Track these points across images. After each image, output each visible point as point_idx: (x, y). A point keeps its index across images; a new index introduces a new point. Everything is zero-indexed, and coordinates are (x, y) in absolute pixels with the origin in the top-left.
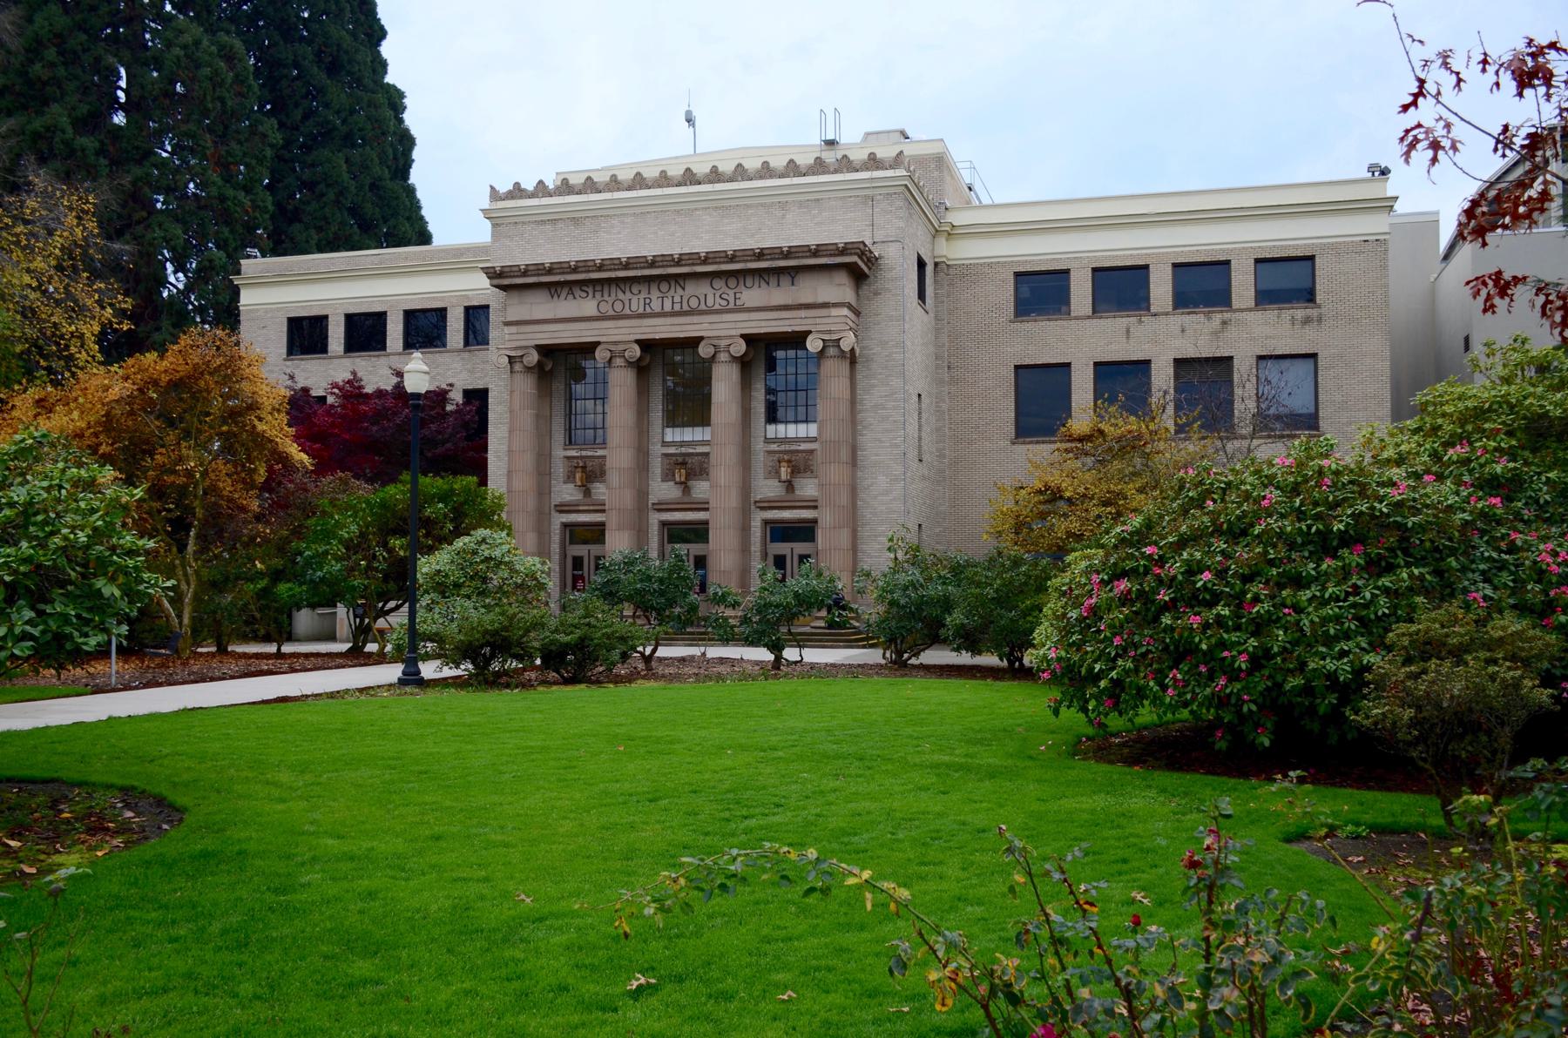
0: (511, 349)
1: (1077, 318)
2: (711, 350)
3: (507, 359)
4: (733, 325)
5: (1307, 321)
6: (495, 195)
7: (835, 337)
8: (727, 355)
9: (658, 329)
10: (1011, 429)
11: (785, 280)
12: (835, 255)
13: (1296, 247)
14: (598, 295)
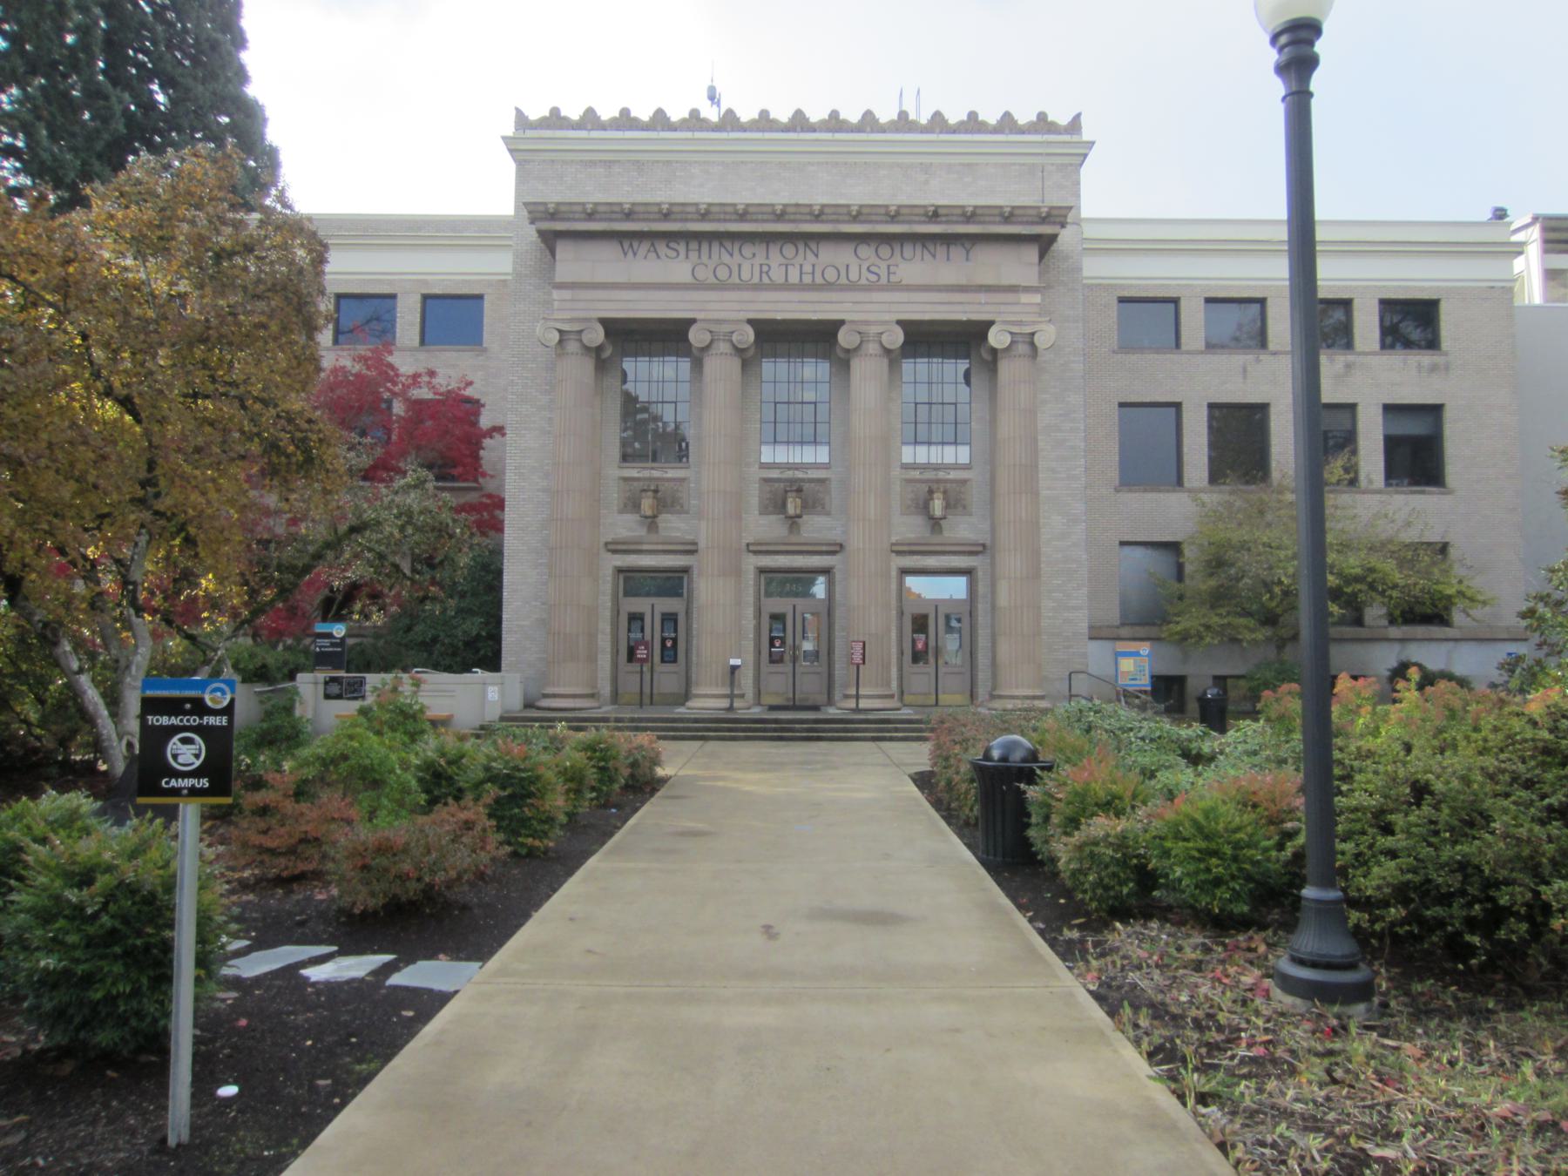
0: (563, 321)
1: (1188, 352)
2: (856, 340)
3: (556, 337)
5: (1434, 368)
6: (521, 120)
7: (1028, 330)
8: (877, 346)
10: (1114, 474)
11: (957, 252)
12: (1033, 223)
13: (1422, 289)
14: (693, 255)
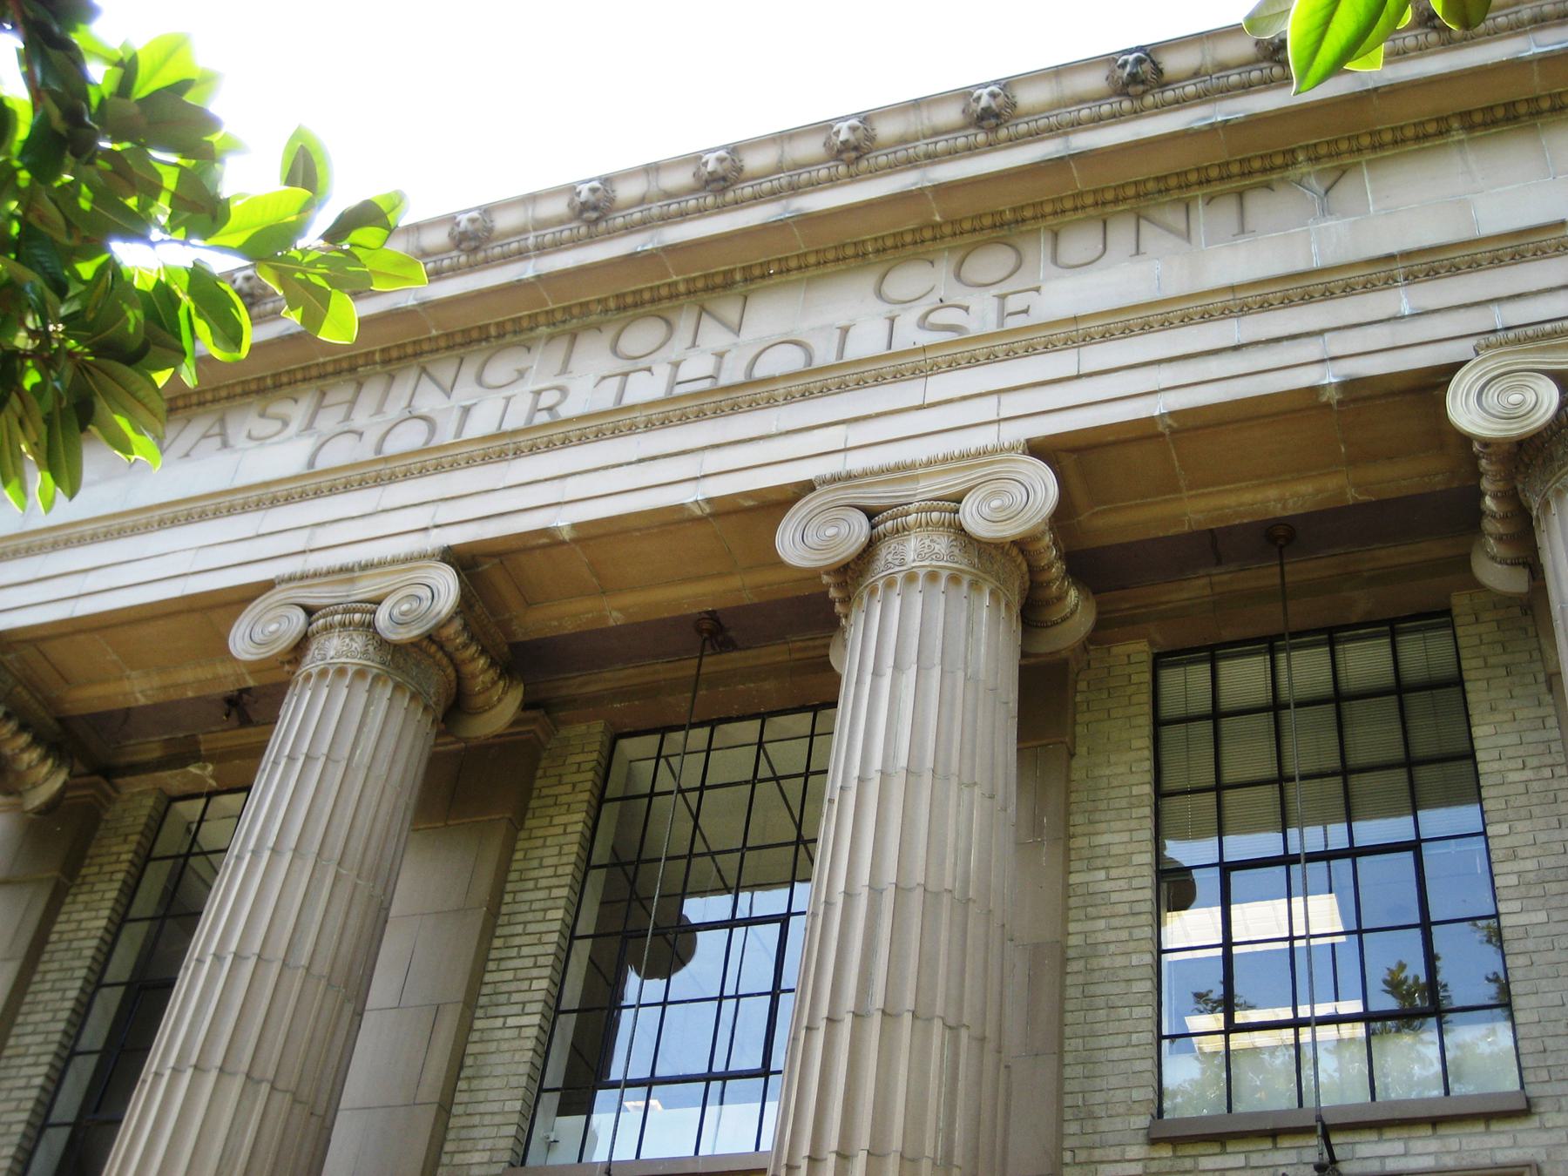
4: (985, 409)
8: (942, 544)
9: (573, 488)
